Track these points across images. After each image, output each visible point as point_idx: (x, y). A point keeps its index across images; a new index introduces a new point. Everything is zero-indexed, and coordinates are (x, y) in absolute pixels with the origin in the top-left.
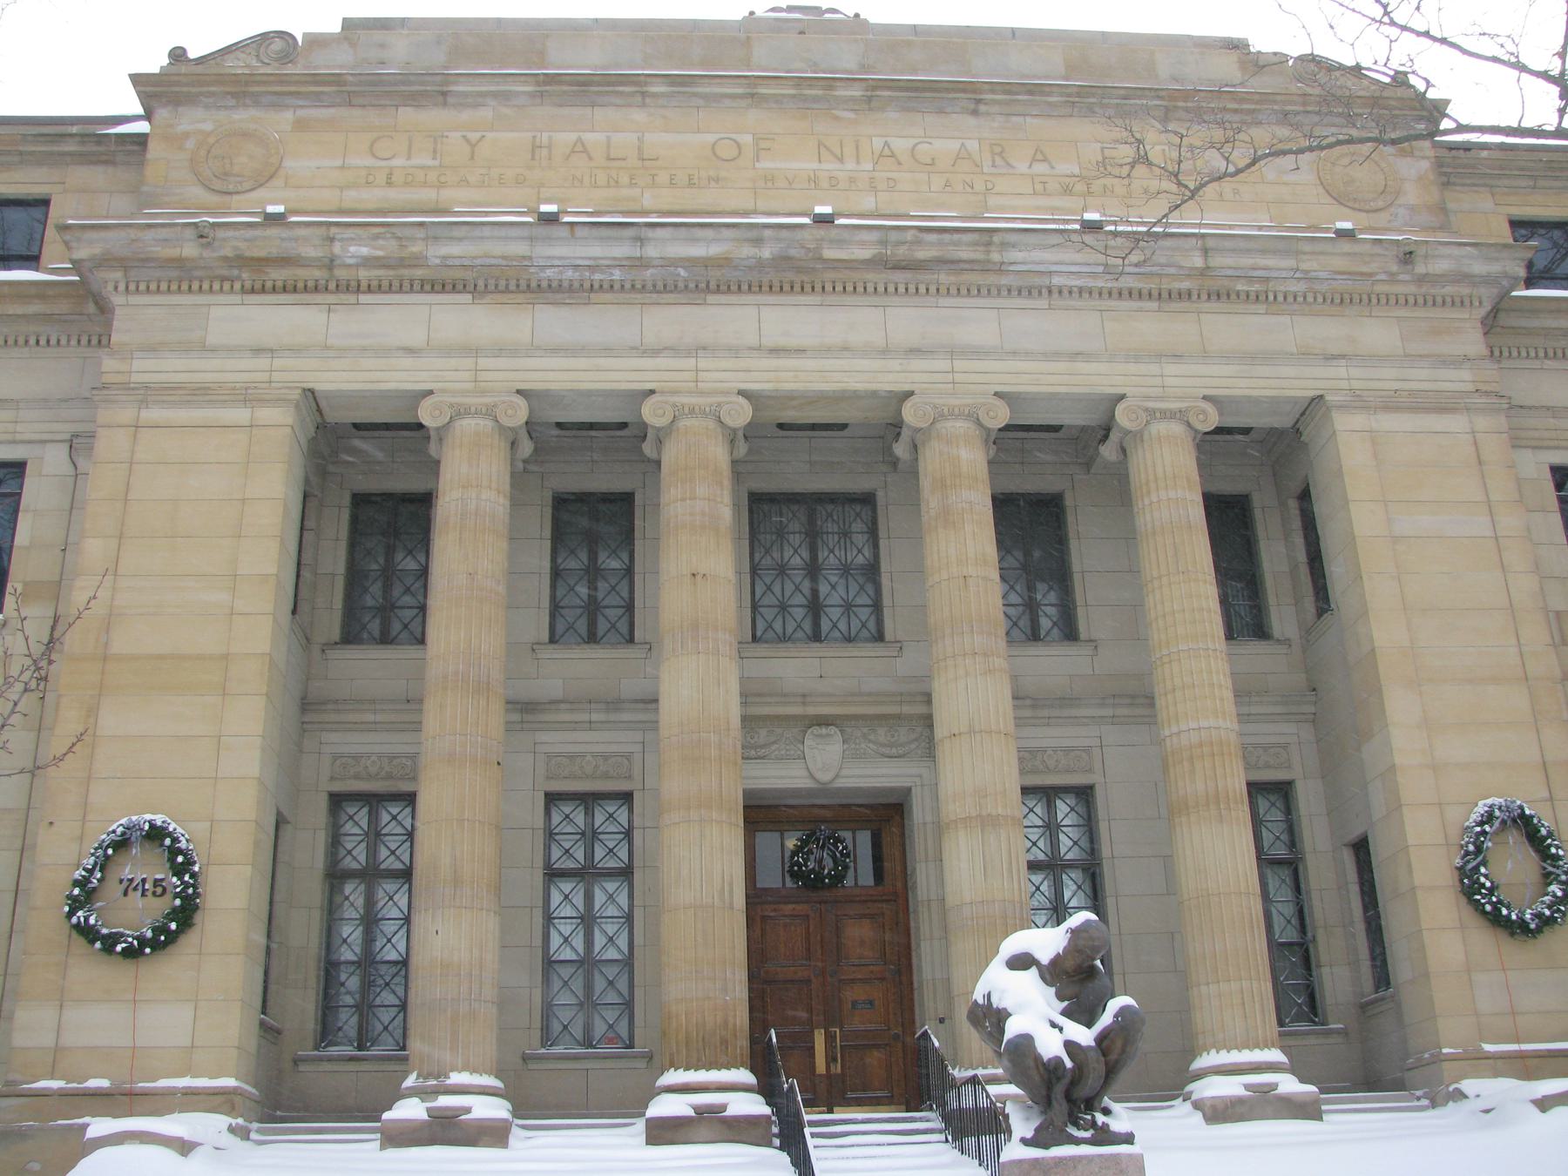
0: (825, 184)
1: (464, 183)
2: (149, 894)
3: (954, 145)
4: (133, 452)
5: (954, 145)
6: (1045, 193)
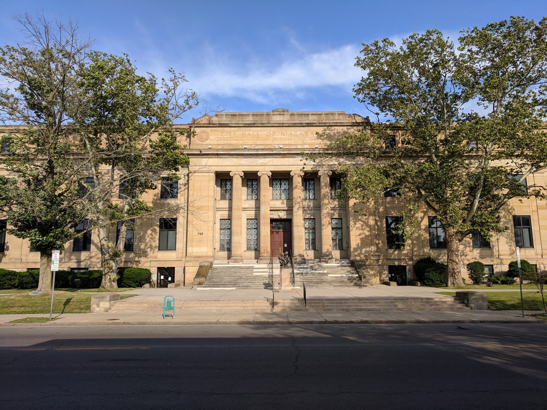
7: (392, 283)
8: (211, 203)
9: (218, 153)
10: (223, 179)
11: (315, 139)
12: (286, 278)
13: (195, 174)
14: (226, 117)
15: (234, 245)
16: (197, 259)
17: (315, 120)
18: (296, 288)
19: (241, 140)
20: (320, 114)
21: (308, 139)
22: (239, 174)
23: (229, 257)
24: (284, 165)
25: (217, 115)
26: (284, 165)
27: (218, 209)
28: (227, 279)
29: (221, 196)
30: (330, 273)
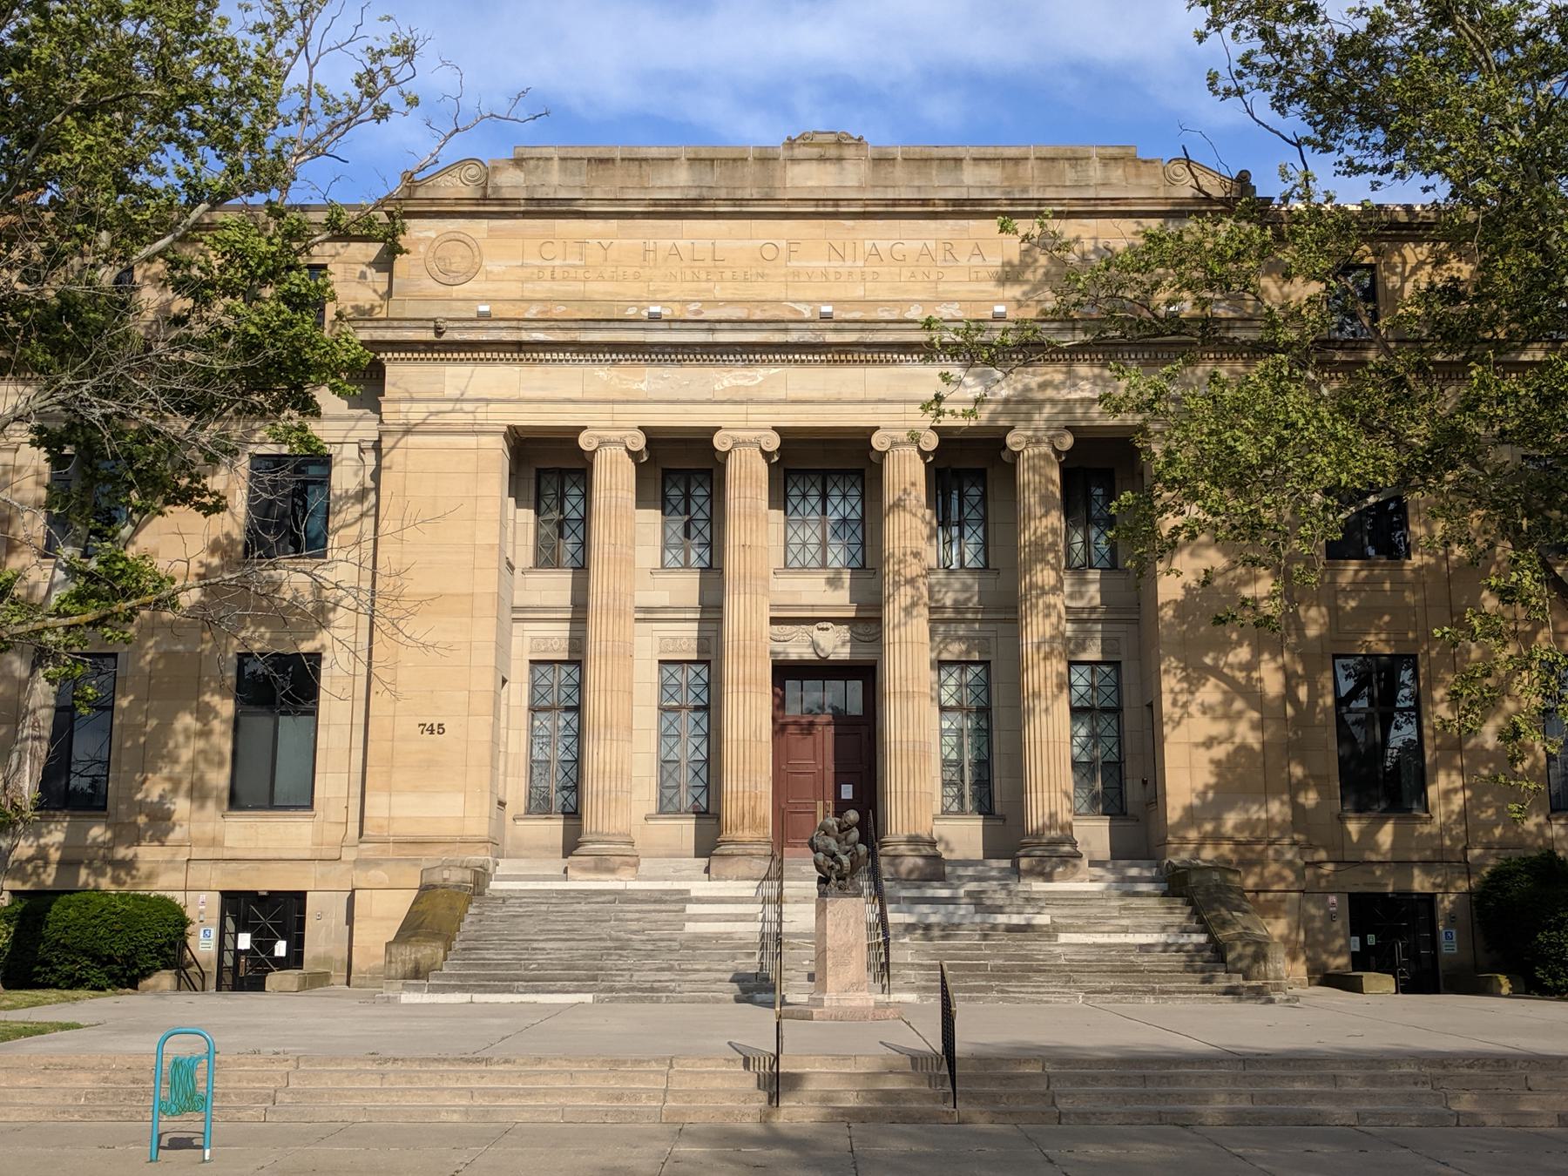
0: (832, 278)
1: (601, 278)
3: (918, 245)
5: (918, 245)
6: (977, 280)
7: (1369, 978)
8: (488, 581)
9: (525, 336)
10: (547, 467)
12: (849, 948)
13: (411, 440)
14: (563, 170)
15: (593, 785)
16: (411, 851)
17: (991, 188)
18: (896, 997)
19: (637, 277)
20: (1016, 160)
21: (963, 272)
22: (622, 442)
23: (571, 845)
24: (838, 401)
25: (518, 162)
26: (838, 401)
27: (521, 614)
28: (554, 950)
30: (1068, 929)
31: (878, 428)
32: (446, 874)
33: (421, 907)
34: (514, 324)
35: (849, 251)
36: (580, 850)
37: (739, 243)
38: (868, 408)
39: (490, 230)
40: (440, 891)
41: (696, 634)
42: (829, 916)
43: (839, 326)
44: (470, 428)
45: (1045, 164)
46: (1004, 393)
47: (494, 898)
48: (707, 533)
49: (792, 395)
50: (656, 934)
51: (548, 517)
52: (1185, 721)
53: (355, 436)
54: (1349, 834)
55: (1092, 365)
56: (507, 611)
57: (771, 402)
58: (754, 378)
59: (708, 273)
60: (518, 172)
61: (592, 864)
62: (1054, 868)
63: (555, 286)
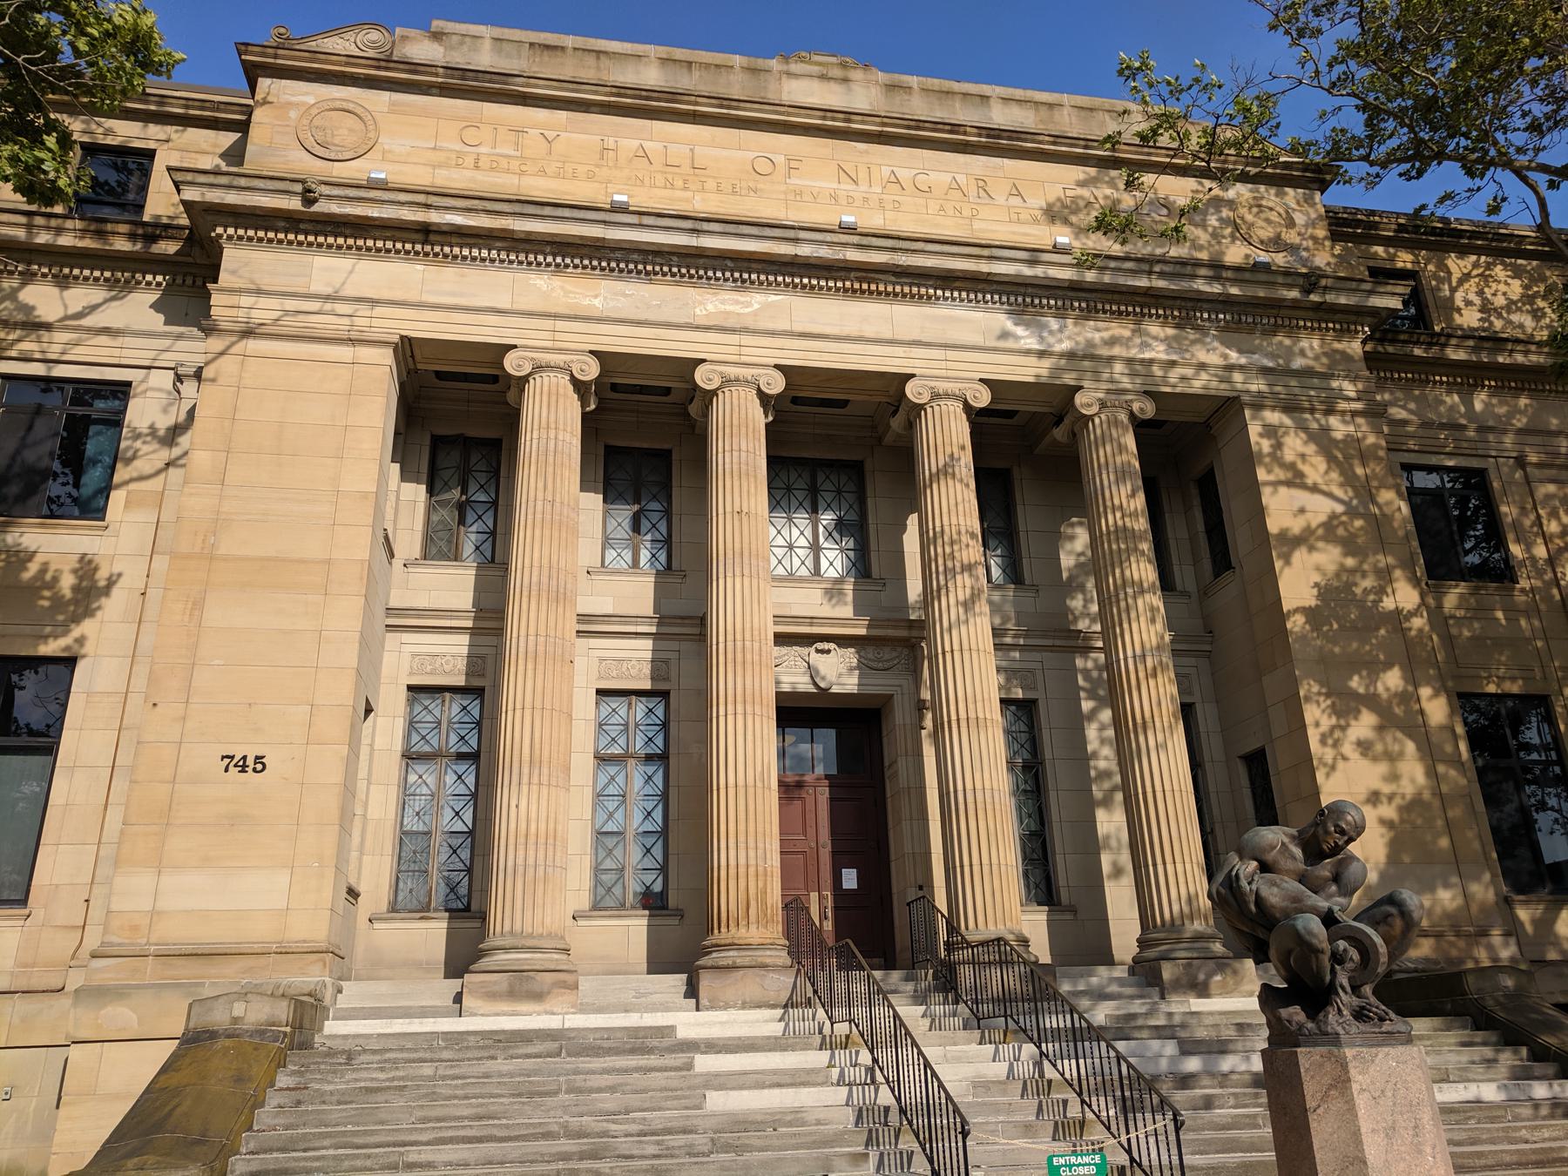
1: (543, 172)
2: (249, 769)
4: (241, 378)
5: (946, 178)
6: (1019, 221)
9: (434, 217)
10: (454, 422)
11: (1036, 221)
13: (252, 345)
15: (509, 853)
16: (185, 971)
19: (591, 177)
20: (1051, 106)
27: (402, 621)
29: (428, 539)
31: (913, 376)
32: (239, 1009)
33: (174, 1080)
34: (421, 198)
35: (863, 175)
36: (484, 963)
37: (725, 153)
38: (899, 351)
39: (392, 104)
40: (222, 1043)
41: (649, 655)
42: (1361, 1102)
43: (865, 241)
44: (345, 335)
45: (1083, 113)
46: (1066, 345)
47: (331, 1053)
48: (663, 527)
49: (798, 328)
50: (657, 1119)
51: (446, 496)
52: (1341, 764)
53: (168, 359)
54: (1522, 924)
55: (1164, 325)
56: (380, 612)
57: (772, 333)
58: (749, 304)
59: (685, 181)
60: (436, 45)
61: (504, 986)
62: (1210, 976)
63: (479, 176)
